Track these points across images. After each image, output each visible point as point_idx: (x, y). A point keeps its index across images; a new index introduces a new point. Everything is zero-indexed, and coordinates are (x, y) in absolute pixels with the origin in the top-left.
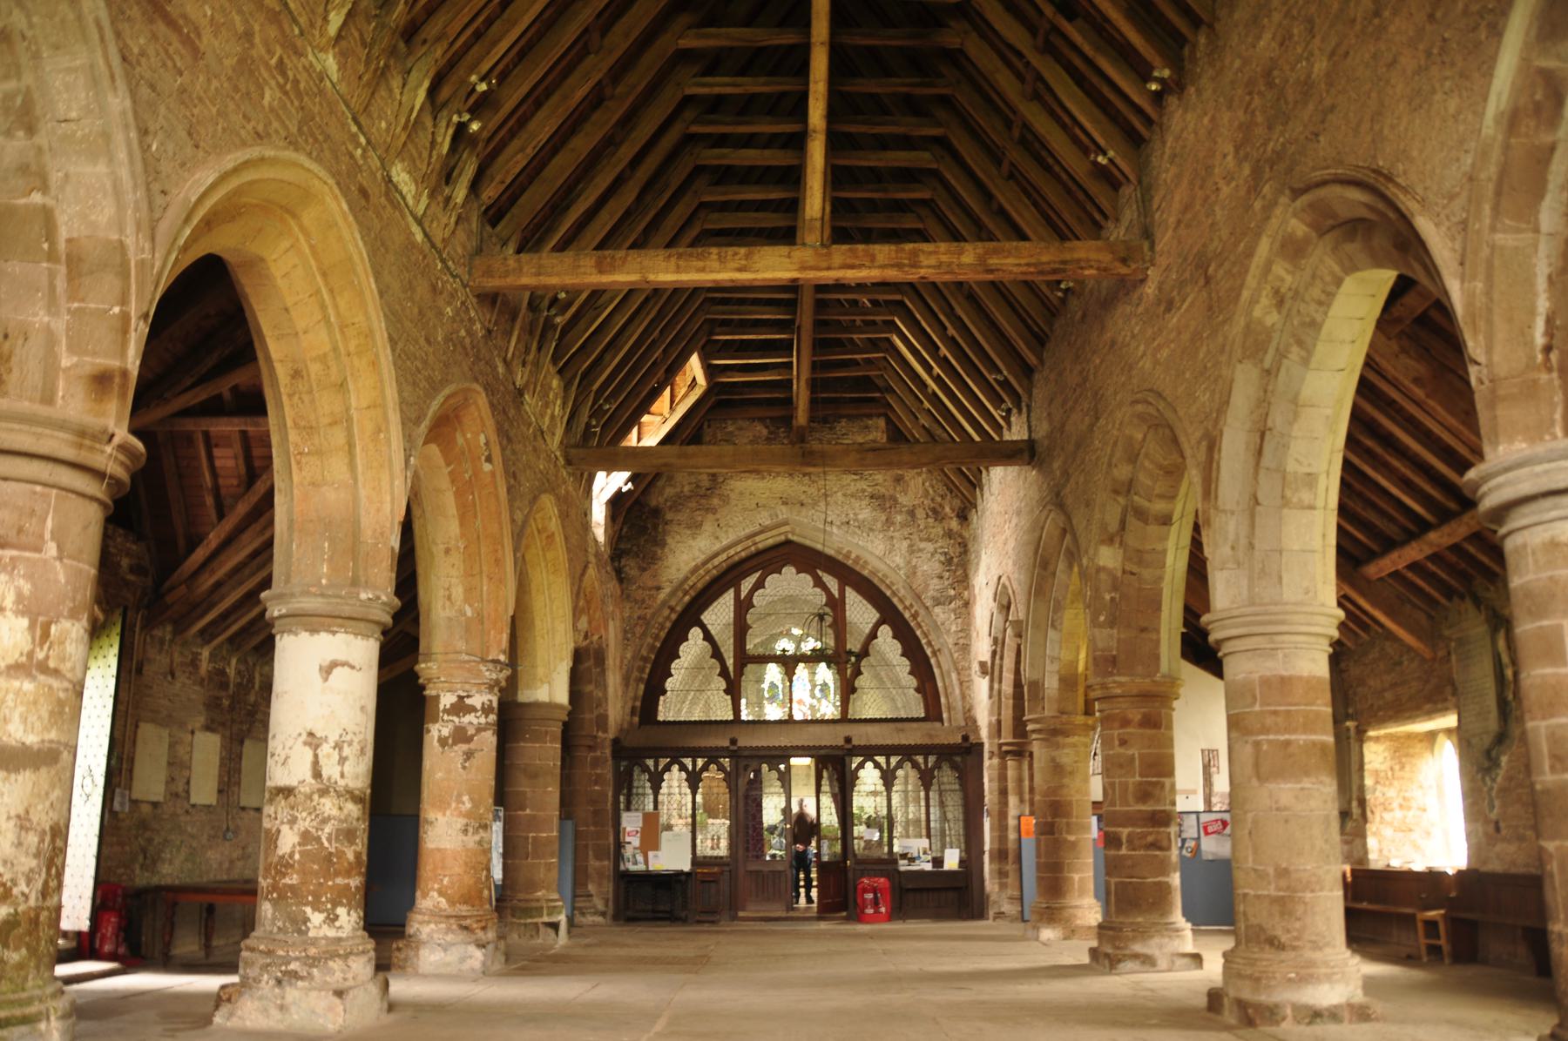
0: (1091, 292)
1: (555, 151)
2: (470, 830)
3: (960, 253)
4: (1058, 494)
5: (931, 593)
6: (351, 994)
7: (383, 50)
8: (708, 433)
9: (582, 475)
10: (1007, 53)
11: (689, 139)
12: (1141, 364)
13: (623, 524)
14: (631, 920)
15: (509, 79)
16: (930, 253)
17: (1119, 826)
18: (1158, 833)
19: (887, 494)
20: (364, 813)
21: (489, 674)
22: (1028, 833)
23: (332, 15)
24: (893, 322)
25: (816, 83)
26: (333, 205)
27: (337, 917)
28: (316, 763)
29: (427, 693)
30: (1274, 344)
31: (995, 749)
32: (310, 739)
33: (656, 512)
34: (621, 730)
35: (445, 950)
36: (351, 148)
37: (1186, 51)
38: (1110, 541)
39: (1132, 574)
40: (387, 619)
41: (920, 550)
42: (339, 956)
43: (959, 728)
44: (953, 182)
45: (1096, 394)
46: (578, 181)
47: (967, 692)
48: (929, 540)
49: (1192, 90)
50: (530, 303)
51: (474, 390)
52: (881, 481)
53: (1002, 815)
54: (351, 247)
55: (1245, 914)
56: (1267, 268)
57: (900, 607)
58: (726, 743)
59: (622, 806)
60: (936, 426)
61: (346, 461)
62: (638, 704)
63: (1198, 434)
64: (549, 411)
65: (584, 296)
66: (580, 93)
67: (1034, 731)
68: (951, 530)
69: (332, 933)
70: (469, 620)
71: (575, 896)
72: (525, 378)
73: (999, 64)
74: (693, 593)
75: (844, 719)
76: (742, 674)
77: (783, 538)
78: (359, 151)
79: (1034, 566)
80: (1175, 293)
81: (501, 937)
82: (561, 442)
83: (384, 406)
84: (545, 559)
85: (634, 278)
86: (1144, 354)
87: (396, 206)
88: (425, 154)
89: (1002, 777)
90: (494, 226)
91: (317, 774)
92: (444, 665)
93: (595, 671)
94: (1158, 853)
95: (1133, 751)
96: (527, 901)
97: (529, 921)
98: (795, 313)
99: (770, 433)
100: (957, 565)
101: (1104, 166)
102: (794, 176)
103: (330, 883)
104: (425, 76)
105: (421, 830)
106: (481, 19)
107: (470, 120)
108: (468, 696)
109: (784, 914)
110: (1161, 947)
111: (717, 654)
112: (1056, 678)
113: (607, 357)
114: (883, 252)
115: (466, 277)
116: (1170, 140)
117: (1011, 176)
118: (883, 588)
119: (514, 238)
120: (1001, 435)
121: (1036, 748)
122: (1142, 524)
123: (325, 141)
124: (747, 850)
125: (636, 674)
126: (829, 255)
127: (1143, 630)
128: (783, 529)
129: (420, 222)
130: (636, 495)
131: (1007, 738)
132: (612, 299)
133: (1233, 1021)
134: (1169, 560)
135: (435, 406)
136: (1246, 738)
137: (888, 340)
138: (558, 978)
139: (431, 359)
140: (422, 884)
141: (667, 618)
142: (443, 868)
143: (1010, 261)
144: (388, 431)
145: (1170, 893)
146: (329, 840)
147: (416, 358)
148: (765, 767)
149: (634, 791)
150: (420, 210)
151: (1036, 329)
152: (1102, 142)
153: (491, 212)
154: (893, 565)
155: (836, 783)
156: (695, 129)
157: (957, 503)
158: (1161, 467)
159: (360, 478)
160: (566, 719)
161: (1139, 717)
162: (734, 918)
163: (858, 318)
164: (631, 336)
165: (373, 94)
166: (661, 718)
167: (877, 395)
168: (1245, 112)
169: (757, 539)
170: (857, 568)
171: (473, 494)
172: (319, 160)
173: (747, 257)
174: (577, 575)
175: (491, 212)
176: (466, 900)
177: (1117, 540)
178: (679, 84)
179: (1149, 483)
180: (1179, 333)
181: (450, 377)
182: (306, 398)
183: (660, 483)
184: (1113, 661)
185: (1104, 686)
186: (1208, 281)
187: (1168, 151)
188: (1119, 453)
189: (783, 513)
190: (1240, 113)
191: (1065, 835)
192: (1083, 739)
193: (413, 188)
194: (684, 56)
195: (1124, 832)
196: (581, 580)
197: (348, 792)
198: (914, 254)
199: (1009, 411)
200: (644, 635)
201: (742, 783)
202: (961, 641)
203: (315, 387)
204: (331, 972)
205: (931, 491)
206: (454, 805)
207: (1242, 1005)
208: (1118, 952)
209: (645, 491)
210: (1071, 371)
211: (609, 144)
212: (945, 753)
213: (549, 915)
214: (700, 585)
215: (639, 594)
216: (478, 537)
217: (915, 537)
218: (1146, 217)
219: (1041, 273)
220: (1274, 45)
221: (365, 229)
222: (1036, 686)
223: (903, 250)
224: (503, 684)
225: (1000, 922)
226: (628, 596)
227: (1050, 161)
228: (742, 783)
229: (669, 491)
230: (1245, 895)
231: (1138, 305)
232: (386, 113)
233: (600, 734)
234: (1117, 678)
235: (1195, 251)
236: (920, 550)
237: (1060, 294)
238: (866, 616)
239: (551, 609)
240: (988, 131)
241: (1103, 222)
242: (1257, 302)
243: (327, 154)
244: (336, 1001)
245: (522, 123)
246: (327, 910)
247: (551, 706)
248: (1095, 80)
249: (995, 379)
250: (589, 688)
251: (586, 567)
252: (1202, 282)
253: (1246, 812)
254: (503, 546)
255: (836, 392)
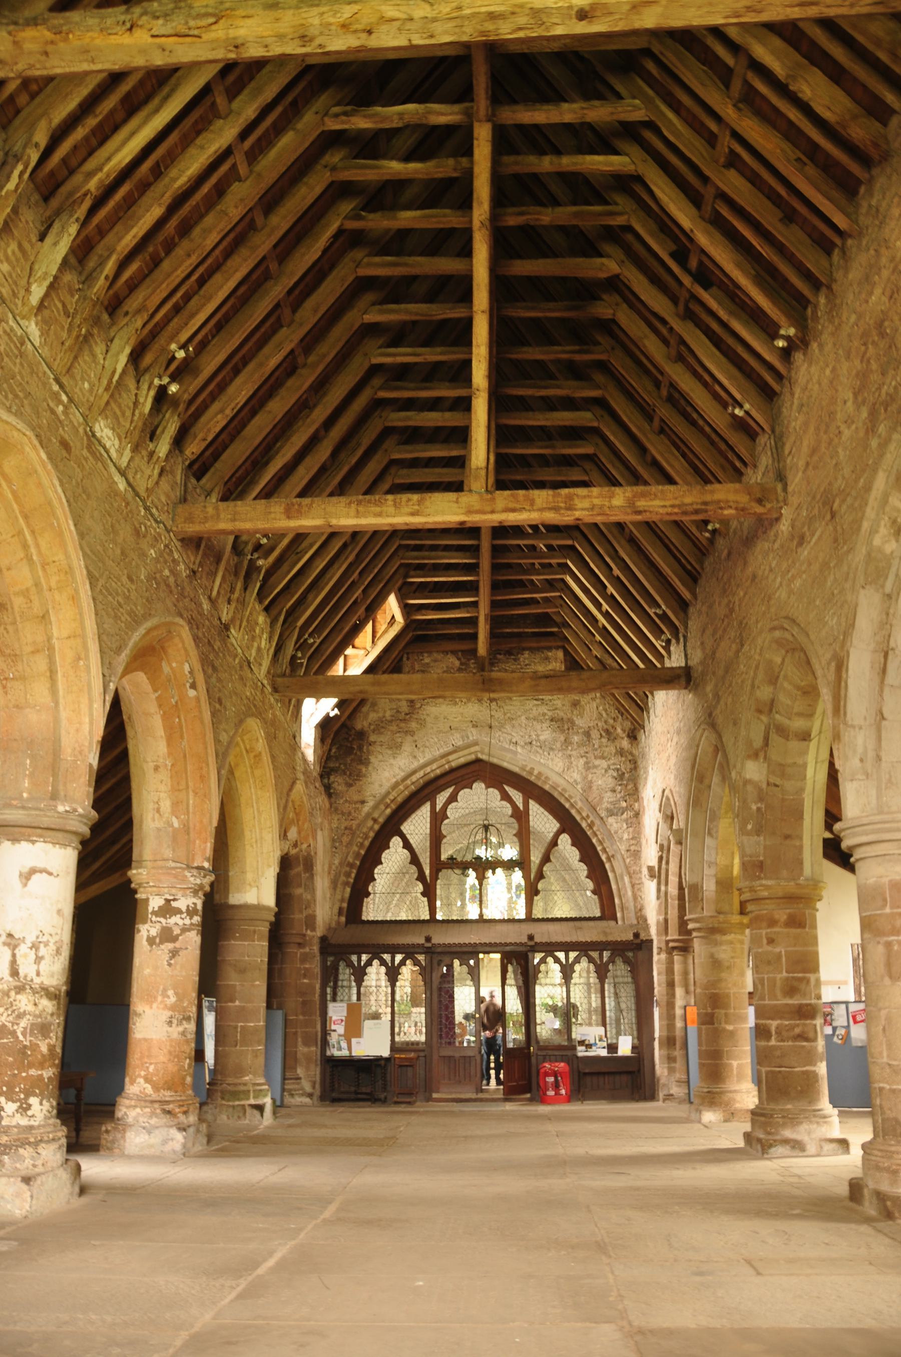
0: (735, 533)
1: (254, 413)
2: (175, 1021)
3: (611, 497)
4: (710, 715)
5: (605, 805)
6: (39, 1180)
7: (85, 319)
8: (407, 664)
9: (290, 701)
10: (653, 320)
11: (378, 404)
12: (777, 595)
13: (332, 745)
14: (335, 1100)
15: (209, 347)
16: (584, 497)
17: (769, 1019)
18: (805, 1025)
19: (565, 717)
20: (58, 1009)
21: (193, 879)
22: (693, 1022)
23: (34, 287)
24: (566, 564)
25: (478, 346)
26: (32, 455)
27: (29, 1107)
28: (14, 962)
29: (138, 896)
30: (893, 570)
31: (663, 946)
32: (9, 940)
33: (361, 735)
34: (329, 928)
35: (149, 1133)
36: (52, 404)
37: (809, 311)
38: (755, 755)
39: (776, 786)
40: (85, 830)
41: (595, 767)
42: (29, 1144)
43: (631, 926)
44: (612, 438)
45: (741, 623)
46: (276, 440)
47: (639, 893)
48: (603, 757)
49: (814, 345)
50: (235, 547)
51: (177, 624)
52: (560, 705)
53: (670, 1005)
54: (51, 494)
55: (881, 1107)
56: (885, 501)
57: (578, 818)
58: (422, 941)
59: (329, 997)
60: (606, 656)
61: (48, 685)
62: (345, 905)
63: (828, 656)
64: (256, 644)
65: (285, 542)
66: (274, 362)
67: (694, 930)
68: (622, 749)
69: (24, 1122)
70: (175, 831)
71: (284, 1079)
72: (230, 615)
73: (647, 330)
74: (394, 806)
75: (529, 919)
76: (437, 879)
77: (473, 757)
78: (61, 408)
79: (692, 780)
80: (806, 528)
81: (201, 1120)
82: (269, 672)
83: (84, 637)
84: (253, 776)
85: (318, 522)
86: (781, 584)
87: (98, 458)
88: (128, 413)
89: (670, 971)
90: (198, 479)
91: (15, 973)
92: (153, 871)
93: (305, 876)
94: (805, 1044)
95: (780, 949)
96: (235, 1085)
97: (237, 1103)
98: (478, 558)
99: (462, 664)
100: (629, 780)
101: (741, 418)
102: (462, 435)
103: (24, 1074)
104: (127, 343)
105: (131, 1022)
106: (179, 295)
107: (169, 383)
108: (174, 900)
109: (474, 1096)
110: (809, 1133)
111: (415, 860)
112: (713, 881)
113: (310, 597)
114: (541, 496)
115: (169, 523)
116: (797, 391)
117: (662, 431)
118: (562, 801)
119: (217, 490)
120: (662, 663)
121: (697, 945)
122: (783, 740)
123: (26, 397)
124: (441, 1037)
125: (343, 878)
126: (493, 499)
127: (787, 837)
128: (473, 749)
129: (123, 473)
130: (342, 720)
131: (673, 935)
132: (311, 546)
133: (873, 1213)
134: (810, 772)
135: (136, 637)
136: (878, 939)
137: (563, 580)
138: (251, 1160)
139: (133, 595)
140: (130, 1071)
141: (370, 829)
142: (149, 1056)
143: (657, 503)
144: (87, 658)
145: (817, 1081)
146: (24, 1034)
147: (118, 594)
148: (456, 963)
149: (340, 983)
150: (124, 462)
151: (689, 567)
152: (738, 396)
153: (196, 467)
154: (571, 781)
155: (519, 976)
156: (383, 394)
157: (628, 725)
158: (798, 688)
159: (61, 701)
160: (273, 919)
161: (785, 917)
162: (429, 1099)
163: (536, 561)
164: (330, 579)
165: (76, 358)
166: (364, 918)
167: (555, 629)
168: (862, 361)
169: (451, 758)
170: (540, 784)
171: (179, 717)
172: (18, 414)
173: (420, 503)
174: (285, 791)
175: (196, 467)
176: (169, 1086)
177: (762, 755)
178: (366, 355)
179: (789, 702)
180: (810, 564)
181: (153, 612)
182: (10, 628)
183: (365, 709)
184: (761, 866)
185: (752, 890)
186: (833, 516)
187: (796, 402)
188: (761, 675)
189: (474, 734)
190: (857, 362)
191: (723, 1025)
192: (739, 937)
193: (117, 442)
194: (370, 330)
195: (774, 1024)
196: (288, 795)
197: (43, 989)
198: (570, 498)
199: (668, 642)
200: (349, 844)
201: (436, 977)
202: (633, 848)
203: (18, 618)
204: (22, 1159)
205: (604, 715)
206: (160, 998)
207: (880, 1197)
208: (770, 1137)
209: (352, 716)
210: (720, 604)
211: (303, 407)
212: (619, 949)
213: (254, 1098)
214: (400, 799)
215: (346, 808)
216: (185, 756)
217: (590, 755)
218: (779, 462)
219: (685, 513)
220: (885, 299)
221: (64, 479)
222: (696, 888)
223: (559, 494)
224: (208, 888)
225: (668, 1103)
226: (336, 809)
227: (695, 416)
228: (436, 977)
229: (373, 716)
230: (881, 1089)
231: (775, 541)
232: (89, 376)
233: (309, 932)
234: (764, 882)
235: (822, 489)
236: (595, 767)
237: (707, 535)
238: (547, 825)
239: (259, 821)
240: (640, 390)
241: (743, 469)
242: (877, 532)
243: (28, 409)
244: (24, 1187)
245: (222, 388)
246: (19, 1100)
247: (259, 908)
248: (730, 341)
249: (655, 613)
250: (299, 891)
251: (294, 783)
252: (828, 517)
253: (880, 1010)
254: (208, 765)
255: (519, 627)
